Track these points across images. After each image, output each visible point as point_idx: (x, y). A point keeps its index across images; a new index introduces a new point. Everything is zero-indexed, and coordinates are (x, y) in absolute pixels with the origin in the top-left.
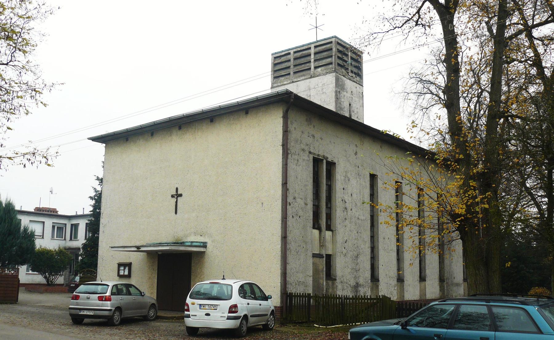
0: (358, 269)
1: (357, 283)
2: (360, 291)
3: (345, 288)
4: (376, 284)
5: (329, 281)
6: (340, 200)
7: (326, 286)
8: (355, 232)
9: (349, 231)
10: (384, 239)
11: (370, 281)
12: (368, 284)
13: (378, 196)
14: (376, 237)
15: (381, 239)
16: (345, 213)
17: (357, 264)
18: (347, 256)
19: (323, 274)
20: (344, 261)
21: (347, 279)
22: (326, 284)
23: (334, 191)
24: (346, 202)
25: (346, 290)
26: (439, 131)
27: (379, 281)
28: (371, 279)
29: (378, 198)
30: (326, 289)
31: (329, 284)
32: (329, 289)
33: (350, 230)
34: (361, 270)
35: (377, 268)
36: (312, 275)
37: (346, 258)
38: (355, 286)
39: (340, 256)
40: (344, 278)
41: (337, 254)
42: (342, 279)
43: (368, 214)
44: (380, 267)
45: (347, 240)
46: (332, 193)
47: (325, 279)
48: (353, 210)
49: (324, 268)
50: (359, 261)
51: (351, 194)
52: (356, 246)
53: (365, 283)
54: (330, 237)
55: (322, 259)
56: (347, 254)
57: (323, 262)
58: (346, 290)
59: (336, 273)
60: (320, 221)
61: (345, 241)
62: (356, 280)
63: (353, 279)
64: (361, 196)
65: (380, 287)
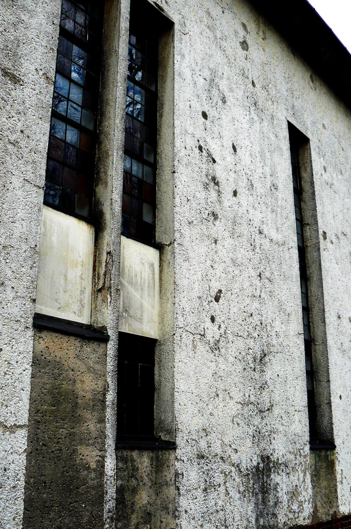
0: (267, 405)
1: (266, 459)
2: (275, 489)
3: (219, 479)
4: (327, 456)
5: (135, 454)
6: (191, 143)
7: (118, 476)
8: (254, 274)
9: (228, 261)
10: (339, 317)
11: (307, 448)
12: (302, 459)
13: (313, 193)
14: (315, 311)
15: (330, 318)
16: (214, 194)
17: (262, 388)
18: (223, 351)
19: (102, 420)
20: (211, 372)
21: (223, 444)
22: (118, 469)
23: (166, 109)
24: (214, 161)
25: (222, 489)
26: (267, 491)
27: (334, 447)
28: (311, 442)
29: (314, 199)
30: (120, 491)
31: (135, 469)
32: (134, 491)
33: (234, 261)
34: (276, 411)
35: (324, 407)
36: (24, 418)
37: (221, 360)
38: (257, 468)
39: (195, 347)
40: (212, 437)
41: (177, 337)
42: (203, 444)
43: (290, 232)
44: (335, 400)
45: (220, 291)
46: (161, 116)
47: (110, 442)
48: (243, 197)
49: (105, 390)
50: (268, 375)
51: (234, 148)
52: (256, 320)
53: (292, 457)
54: (147, 268)
55: (95, 345)
56: (221, 344)
57: (104, 363)
58: (222, 489)
59: (174, 417)
60: (100, 189)
61: (214, 294)
62: (262, 445)
63: (249, 443)
64: (267, 170)
65: (338, 468)
